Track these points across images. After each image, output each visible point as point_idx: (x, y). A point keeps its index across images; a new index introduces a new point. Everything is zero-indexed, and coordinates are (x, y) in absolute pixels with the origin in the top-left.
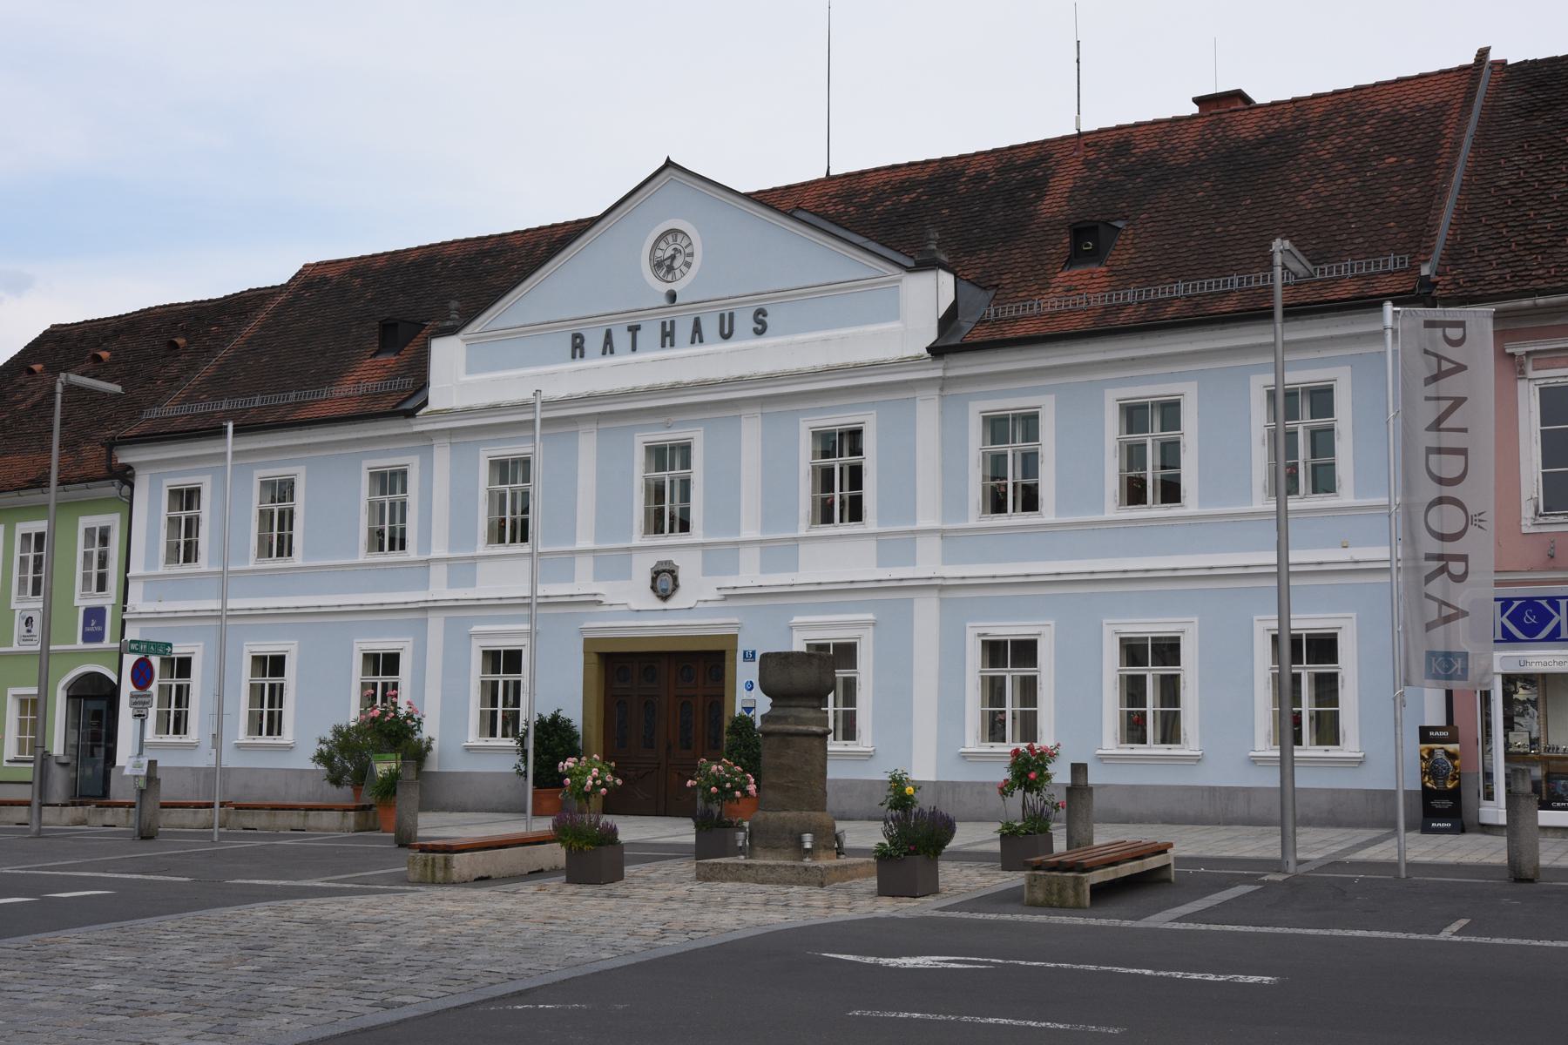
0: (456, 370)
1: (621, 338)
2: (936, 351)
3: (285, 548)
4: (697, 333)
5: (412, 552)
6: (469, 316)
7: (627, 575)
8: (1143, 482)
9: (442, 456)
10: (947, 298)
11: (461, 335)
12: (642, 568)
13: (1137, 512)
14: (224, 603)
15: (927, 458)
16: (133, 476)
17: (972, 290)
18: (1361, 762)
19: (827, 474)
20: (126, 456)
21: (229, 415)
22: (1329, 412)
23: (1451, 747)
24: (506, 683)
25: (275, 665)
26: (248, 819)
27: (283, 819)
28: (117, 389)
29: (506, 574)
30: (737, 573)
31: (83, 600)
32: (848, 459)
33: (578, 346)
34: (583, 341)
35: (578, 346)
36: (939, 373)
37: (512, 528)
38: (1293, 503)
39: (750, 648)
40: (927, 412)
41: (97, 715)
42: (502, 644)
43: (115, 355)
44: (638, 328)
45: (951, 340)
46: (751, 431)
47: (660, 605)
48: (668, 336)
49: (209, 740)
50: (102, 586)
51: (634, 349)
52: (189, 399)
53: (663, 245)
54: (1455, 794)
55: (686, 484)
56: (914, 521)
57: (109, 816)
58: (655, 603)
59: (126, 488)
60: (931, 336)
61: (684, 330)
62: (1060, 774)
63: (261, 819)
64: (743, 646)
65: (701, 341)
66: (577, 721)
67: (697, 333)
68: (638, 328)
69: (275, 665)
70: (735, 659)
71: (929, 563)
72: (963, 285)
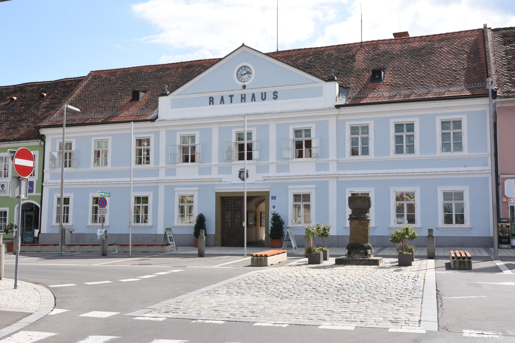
4: (222, 100)
11: (169, 96)
13: (400, 156)
18: (471, 229)
23: (508, 224)
24: (64, 207)
30: (269, 172)
33: (211, 100)
35: (211, 100)
39: (274, 195)
43: (18, 99)
44: (233, 96)
47: (242, 182)
48: (243, 98)
51: (231, 102)
53: (241, 70)
56: (211, 162)
59: (42, 143)
61: (249, 98)
64: (271, 195)
65: (224, 103)
67: (222, 100)
68: (233, 96)
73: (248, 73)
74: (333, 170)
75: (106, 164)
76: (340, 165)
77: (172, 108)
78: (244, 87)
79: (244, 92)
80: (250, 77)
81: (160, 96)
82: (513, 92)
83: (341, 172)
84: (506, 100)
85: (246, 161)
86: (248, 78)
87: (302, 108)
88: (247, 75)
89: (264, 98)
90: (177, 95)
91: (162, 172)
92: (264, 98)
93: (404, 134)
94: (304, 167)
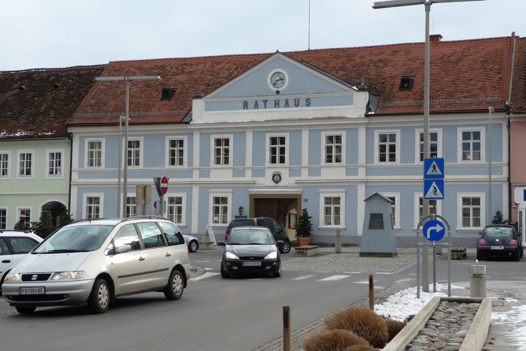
7: (264, 175)
8: (331, 156)
11: (203, 99)
12: (269, 174)
14: (490, 176)
15: (363, 146)
16: (72, 136)
17: (374, 97)
18: (400, 230)
20: (70, 130)
21: (490, 103)
22: (479, 139)
29: (222, 174)
32: (97, 150)
34: (247, 103)
36: (367, 122)
38: (129, 168)
47: (275, 185)
53: (274, 76)
58: (273, 184)
59: (70, 140)
61: (282, 103)
70: (301, 201)
72: (371, 95)
73: (282, 79)
74: (362, 175)
75: (99, 165)
76: (369, 171)
77: (206, 110)
78: (278, 92)
79: (277, 97)
80: (283, 83)
81: (193, 98)
82: (525, 109)
83: (371, 178)
84: (517, 115)
85: (278, 164)
86: (282, 84)
87: (277, 117)
88: (280, 82)
89: (297, 104)
90: (211, 98)
91: (196, 173)
92: (297, 104)
93: (471, 142)
94: (334, 173)
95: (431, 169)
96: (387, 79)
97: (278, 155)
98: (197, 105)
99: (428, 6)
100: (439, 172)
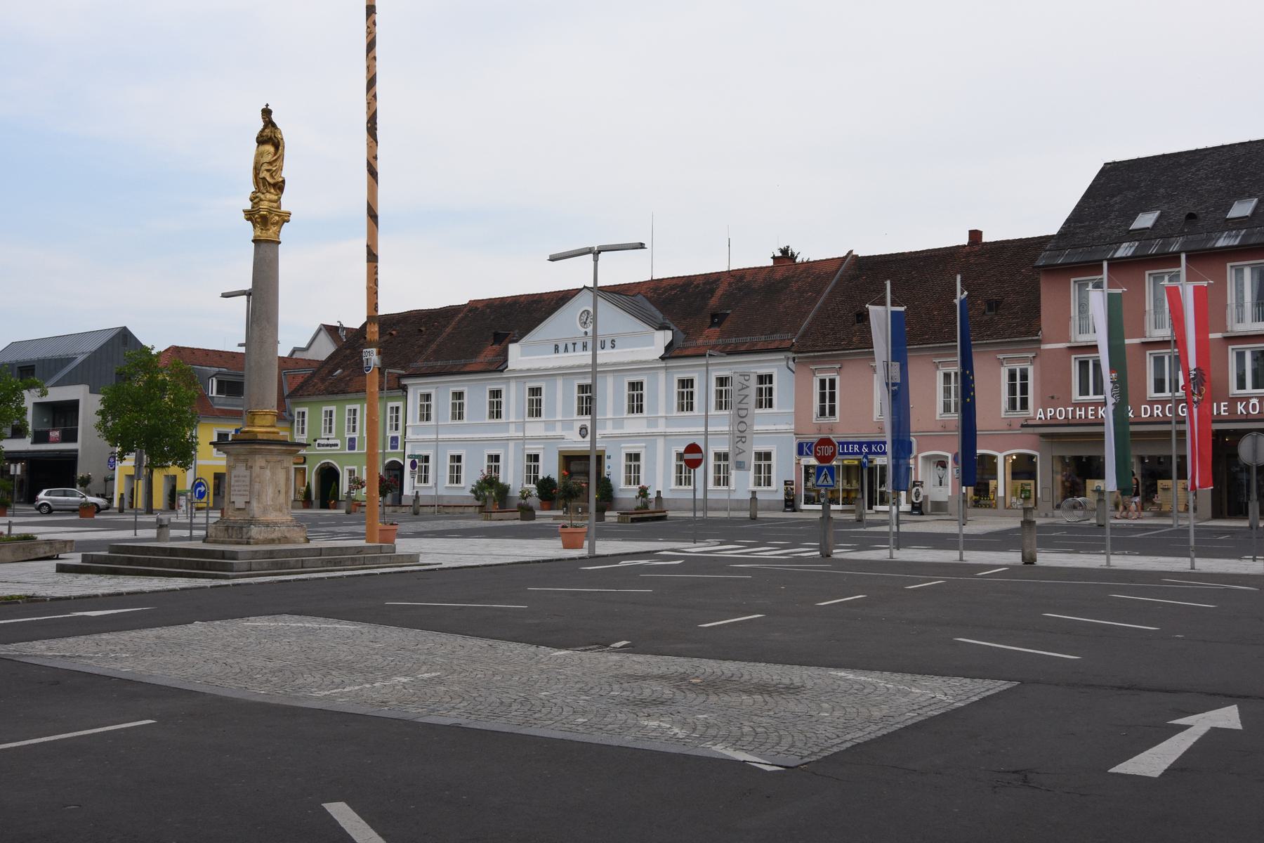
0: (519, 357)
1: (570, 347)
2: (662, 358)
3: (461, 417)
4: (566, 350)
5: (503, 420)
6: (522, 336)
7: (572, 429)
9: (513, 385)
10: (670, 338)
15: (662, 390)
19: (761, 390)
20: (404, 382)
25: (458, 458)
26: (447, 510)
27: (457, 510)
28: (888, 283)
29: (535, 428)
31: (390, 434)
35: (557, 349)
37: (535, 411)
40: (662, 376)
41: (396, 476)
42: (534, 452)
45: (671, 352)
46: (560, 382)
49: (439, 485)
50: (354, 430)
52: (427, 360)
54: (793, 501)
55: (771, 389)
57: (404, 509)
58: (581, 439)
60: (663, 352)
62: (653, 495)
63: (451, 510)
66: (557, 479)
69: (459, 458)
71: (661, 428)
94: (636, 425)
95: (822, 478)
96: (706, 314)
97: (587, 404)
98: (514, 349)
99: (372, 318)
100: (831, 483)
